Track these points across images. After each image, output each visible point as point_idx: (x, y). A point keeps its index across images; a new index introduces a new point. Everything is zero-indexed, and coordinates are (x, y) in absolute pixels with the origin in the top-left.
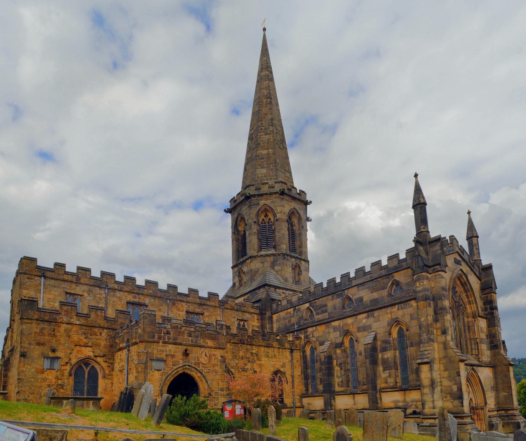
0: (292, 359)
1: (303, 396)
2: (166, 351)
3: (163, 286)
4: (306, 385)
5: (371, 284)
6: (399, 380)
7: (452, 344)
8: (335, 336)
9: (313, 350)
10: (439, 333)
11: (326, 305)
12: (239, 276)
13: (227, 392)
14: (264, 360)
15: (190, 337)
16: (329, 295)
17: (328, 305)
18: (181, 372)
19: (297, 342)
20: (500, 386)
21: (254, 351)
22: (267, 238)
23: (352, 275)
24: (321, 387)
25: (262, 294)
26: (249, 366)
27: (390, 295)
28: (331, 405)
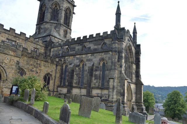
0: (56, 69)
1: (58, 87)
4: (61, 82)
5: (95, 42)
6: (100, 84)
7: (123, 72)
8: (77, 62)
9: (66, 66)
10: (119, 67)
11: (75, 48)
12: (39, 29)
14: (43, 68)
19: (60, 62)
20: (138, 92)
21: (38, 63)
22: (55, 15)
23: (88, 37)
24: (67, 84)
25: (48, 39)
26: (35, 69)
27: (102, 48)
28: (70, 92)
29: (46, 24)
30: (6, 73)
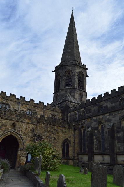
3: (18, 97)
4: (81, 148)
8: (94, 124)
9: (85, 130)
11: (91, 109)
16: (92, 105)
17: (92, 109)
18: (9, 134)
19: (77, 126)
21: (55, 129)
24: (87, 150)
26: (52, 136)
27: (120, 105)
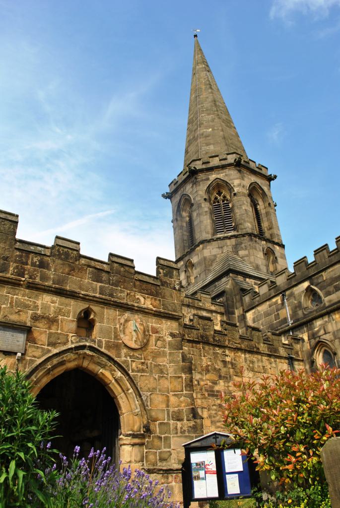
2: (36, 307)
13: (192, 423)
15: (98, 281)
18: (71, 365)
19: (298, 347)
21: (228, 359)
22: (223, 217)
26: (221, 386)
29: (206, 246)
30: (140, 396)
